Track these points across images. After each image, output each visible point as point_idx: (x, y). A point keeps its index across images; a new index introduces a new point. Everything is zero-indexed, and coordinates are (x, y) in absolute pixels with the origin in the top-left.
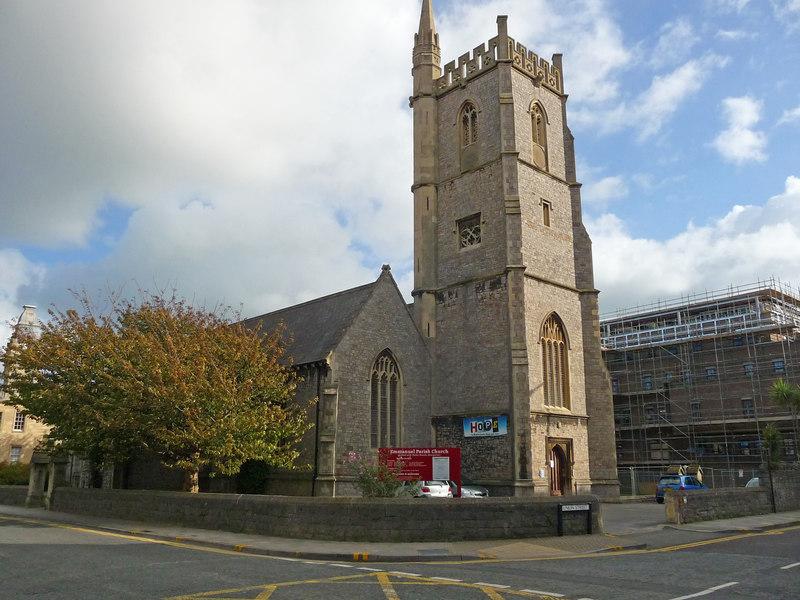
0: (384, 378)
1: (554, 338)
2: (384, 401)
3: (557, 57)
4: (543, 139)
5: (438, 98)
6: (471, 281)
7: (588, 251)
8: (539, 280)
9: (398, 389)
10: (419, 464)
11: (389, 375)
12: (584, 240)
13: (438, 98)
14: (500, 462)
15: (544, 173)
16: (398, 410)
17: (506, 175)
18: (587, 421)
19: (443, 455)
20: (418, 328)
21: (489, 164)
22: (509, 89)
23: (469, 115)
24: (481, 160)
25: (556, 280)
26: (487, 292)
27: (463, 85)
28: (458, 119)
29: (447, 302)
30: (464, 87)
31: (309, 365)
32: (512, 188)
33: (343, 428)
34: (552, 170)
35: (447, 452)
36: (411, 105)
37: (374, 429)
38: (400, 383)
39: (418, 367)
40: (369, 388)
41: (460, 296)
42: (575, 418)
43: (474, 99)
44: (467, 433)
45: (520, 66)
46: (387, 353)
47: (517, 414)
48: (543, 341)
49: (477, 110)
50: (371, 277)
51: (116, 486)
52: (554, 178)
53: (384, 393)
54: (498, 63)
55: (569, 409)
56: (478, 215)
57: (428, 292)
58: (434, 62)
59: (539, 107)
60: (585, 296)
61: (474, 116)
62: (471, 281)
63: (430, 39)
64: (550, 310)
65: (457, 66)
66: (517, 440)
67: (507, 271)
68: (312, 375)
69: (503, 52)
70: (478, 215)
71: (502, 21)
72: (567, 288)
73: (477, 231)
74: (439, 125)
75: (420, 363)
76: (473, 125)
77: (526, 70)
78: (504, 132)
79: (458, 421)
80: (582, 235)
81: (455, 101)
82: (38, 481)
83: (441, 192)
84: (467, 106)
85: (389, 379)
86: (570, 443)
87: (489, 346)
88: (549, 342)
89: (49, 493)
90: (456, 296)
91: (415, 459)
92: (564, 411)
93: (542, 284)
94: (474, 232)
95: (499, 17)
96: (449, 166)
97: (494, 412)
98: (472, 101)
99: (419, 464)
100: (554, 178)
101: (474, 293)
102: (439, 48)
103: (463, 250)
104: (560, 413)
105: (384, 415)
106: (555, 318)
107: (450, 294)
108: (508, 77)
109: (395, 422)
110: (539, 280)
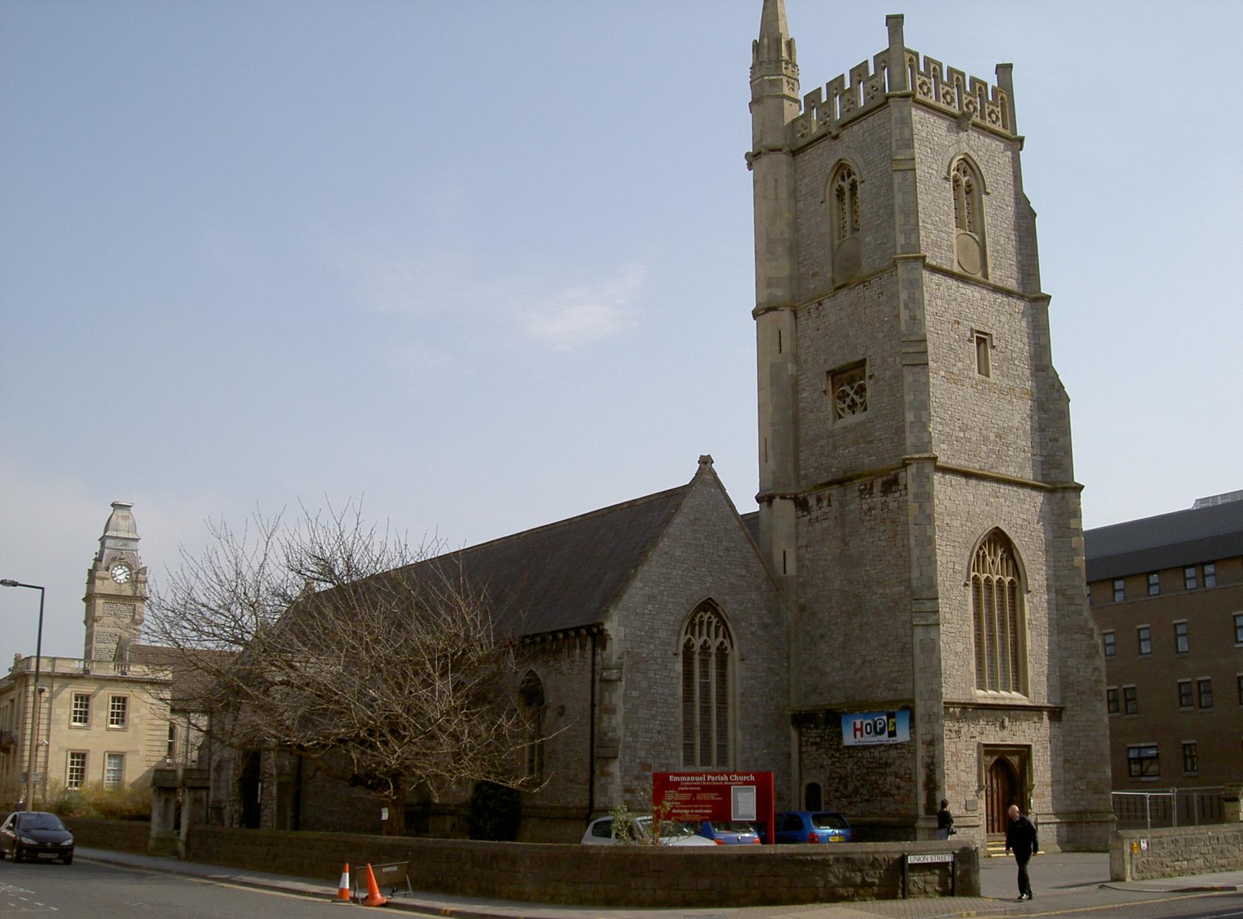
0: (705, 648)
1: (996, 573)
2: (705, 688)
3: (1004, 70)
4: (978, 223)
5: (794, 153)
6: (850, 479)
7: (1064, 415)
8: (967, 475)
9: (730, 666)
10: (712, 796)
11: (714, 644)
12: (1056, 395)
13: (794, 153)
14: (899, 788)
15: (977, 283)
16: (730, 700)
17: (903, 296)
18: (1056, 714)
19: (746, 783)
20: (767, 559)
21: (879, 273)
22: (909, 144)
23: (846, 185)
24: (866, 269)
25: (1002, 471)
26: (878, 499)
27: (834, 133)
28: (829, 193)
29: (814, 515)
30: (836, 137)
31: (577, 630)
32: (913, 318)
33: (634, 735)
34: (994, 277)
35: (752, 778)
36: (750, 166)
37: (688, 734)
38: (734, 655)
39: (765, 627)
40: (679, 667)
41: (835, 504)
42: (1039, 709)
43: (855, 162)
44: (849, 739)
45: (931, 100)
46: (708, 605)
47: (920, 710)
48: (976, 579)
49: (857, 178)
50: (682, 475)
51: (281, 826)
52: (996, 289)
53: (705, 674)
54: (887, 98)
55: (1026, 694)
56: (861, 364)
57: (783, 497)
58: (786, 91)
59: (967, 165)
60: (1059, 495)
61: (853, 187)
62: (850, 479)
63: (779, 50)
64: (989, 526)
65: (824, 99)
66: (921, 751)
67: (905, 465)
68: (583, 647)
69: (897, 79)
70: (861, 364)
71: (895, 23)
72: (1023, 485)
73: (861, 390)
74: (797, 202)
75: (767, 621)
76: (853, 203)
77: (942, 105)
78: (899, 219)
79: (833, 719)
80: (1052, 386)
81: (821, 160)
82: (164, 815)
83: (802, 320)
84: (842, 170)
85: (713, 650)
86: (1024, 752)
87: (880, 591)
88: (988, 580)
89: (183, 837)
90: (829, 505)
91: (706, 789)
92: (1016, 698)
93: (973, 482)
94: (856, 393)
95: (888, 18)
96: (815, 275)
97: (891, 703)
98: (849, 162)
99: (712, 796)
100: (996, 289)
101: (857, 500)
102: (795, 66)
103: (840, 423)
104: (1007, 702)
105: (706, 710)
106: (998, 539)
107: (819, 500)
108: (906, 122)
109: (726, 722)
110: (967, 475)
